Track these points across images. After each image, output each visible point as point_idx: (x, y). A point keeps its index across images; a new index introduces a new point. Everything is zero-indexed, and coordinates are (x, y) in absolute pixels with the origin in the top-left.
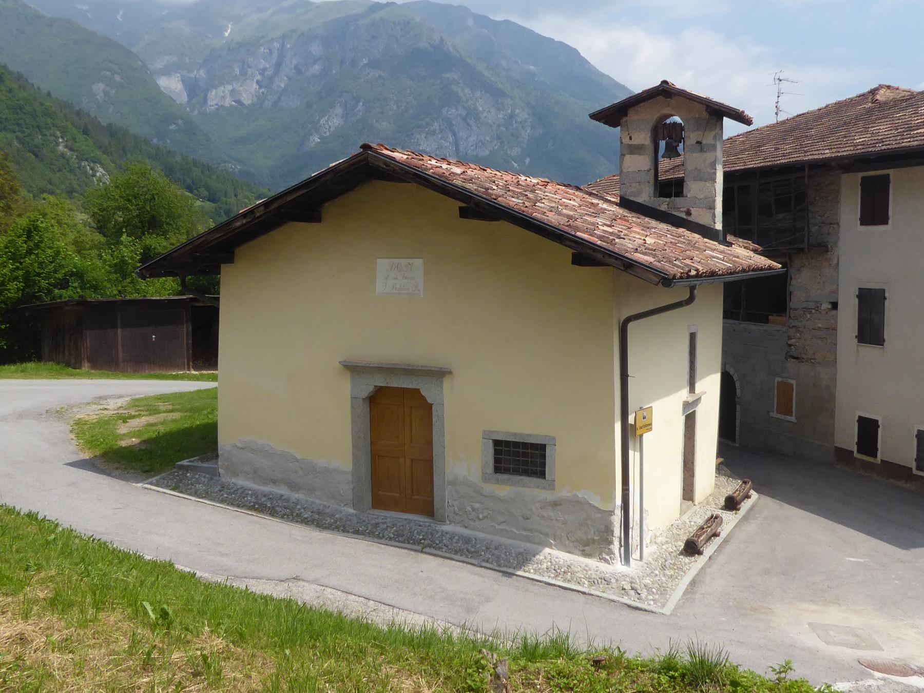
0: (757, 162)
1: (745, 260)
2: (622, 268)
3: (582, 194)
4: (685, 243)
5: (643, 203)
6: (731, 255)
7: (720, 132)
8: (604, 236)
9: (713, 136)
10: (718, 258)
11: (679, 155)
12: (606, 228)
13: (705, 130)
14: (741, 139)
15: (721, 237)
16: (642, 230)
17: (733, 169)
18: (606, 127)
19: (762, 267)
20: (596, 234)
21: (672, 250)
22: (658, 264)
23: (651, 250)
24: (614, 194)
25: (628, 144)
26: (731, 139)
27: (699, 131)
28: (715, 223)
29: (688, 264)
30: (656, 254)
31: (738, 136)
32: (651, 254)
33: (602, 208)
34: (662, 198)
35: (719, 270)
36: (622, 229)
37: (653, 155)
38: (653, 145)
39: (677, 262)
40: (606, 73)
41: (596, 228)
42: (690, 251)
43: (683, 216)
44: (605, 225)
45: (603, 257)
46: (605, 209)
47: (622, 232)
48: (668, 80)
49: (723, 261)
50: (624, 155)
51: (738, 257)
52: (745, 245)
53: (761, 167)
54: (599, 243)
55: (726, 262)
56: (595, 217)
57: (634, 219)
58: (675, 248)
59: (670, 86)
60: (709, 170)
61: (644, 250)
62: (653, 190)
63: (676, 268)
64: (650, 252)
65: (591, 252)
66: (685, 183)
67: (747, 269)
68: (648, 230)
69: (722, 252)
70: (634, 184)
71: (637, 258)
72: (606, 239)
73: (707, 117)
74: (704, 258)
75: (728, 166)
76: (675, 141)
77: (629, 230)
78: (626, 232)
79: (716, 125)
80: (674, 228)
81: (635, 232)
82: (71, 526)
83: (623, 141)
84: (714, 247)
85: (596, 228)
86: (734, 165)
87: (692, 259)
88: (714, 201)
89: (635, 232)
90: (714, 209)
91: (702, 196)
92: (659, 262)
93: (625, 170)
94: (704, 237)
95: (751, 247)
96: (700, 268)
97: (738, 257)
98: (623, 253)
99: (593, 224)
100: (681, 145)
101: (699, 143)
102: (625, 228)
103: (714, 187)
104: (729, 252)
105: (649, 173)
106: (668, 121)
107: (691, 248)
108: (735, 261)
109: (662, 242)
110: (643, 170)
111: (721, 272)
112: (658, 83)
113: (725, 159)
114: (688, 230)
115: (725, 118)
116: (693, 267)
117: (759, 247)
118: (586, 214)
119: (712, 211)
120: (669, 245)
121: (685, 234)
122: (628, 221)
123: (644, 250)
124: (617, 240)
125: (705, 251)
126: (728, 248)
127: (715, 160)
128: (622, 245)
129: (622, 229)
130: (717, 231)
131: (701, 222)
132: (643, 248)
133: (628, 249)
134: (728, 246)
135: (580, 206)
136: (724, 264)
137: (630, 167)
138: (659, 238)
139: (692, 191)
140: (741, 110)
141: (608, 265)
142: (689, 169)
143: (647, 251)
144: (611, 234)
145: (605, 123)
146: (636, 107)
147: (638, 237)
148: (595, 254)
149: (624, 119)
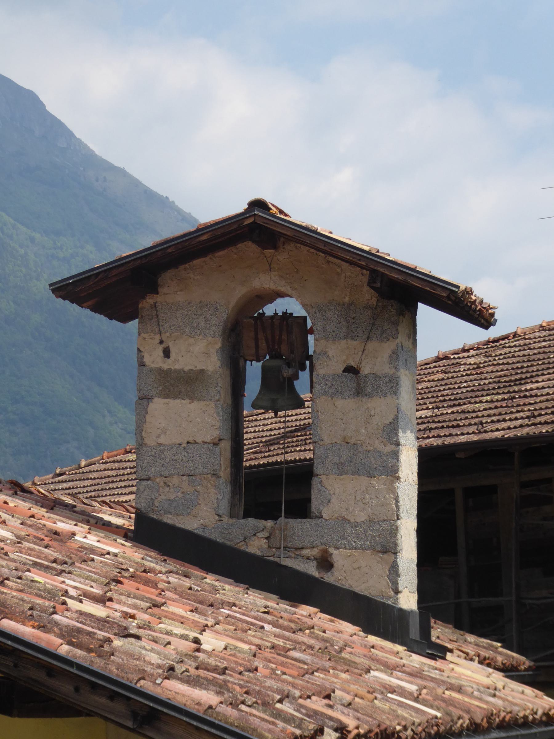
0: (512, 424)
1: (480, 699)
2: (130, 724)
3: (28, 505)
4: (312, 647)
5: (200, 532)
6: (439, 682)
7: (408, 344)
8: (80, 631)
9: (389, 352)
10: (402, 692)
11: (300, 404)
12: (89, 607)
13: (368, 338)
14: (472, 360)
15: (414, 633)
16: (194, 610)
17: (449, 441)
18: (100, 320)
19: (525, 717)
20: (57, 624)
21: (273, 671)
22: (230, 711)
23: (215, 670)
24: (118, 503)
25: (160, 370)
26: (446, 358)
27: (353, 338)
28: (397, 592)
29: (316, 712)
30: (225, 681)
31: (464, 350)
32: (213, 682)
33: (82, 547)
34: (252, 521)
35: (405, 728)
36: (135, 607)
37: (229, 401)
38: (227, 372)
39: (286, 707)
40: (117, 163)
41: (59, 607)
42: (325, 670)
43: (312, 570)
44: (87, 595)
45: (77, 689)
46: (92, 550)
47: (133, 617)
48: (269, 199)
49: (416, 700)
50: (149, 399)
51: (459, 689)
52: (484, 653)
53: (522, 438)
54: (64, 649)
55: (425, 703)
56: (60, 573)
57: (173, 579)
58: (283, 664)
59: (273, 215)
60: (381, 447)
61: (192, 671)
62: (228, 496)
63: (281, 724)
64: (211, 675)
65: (41, 676)
66: (315, 480)
67: (485, 724)
68: (210, 611)
69: (416, 674)
70: (175, 480)
71: (170, 695)
72: (85, 639)
73: (374, 301)
74: (363, 691)
75: (435, 433)
76: (289, 365)
77: (156, 610)
78: (146, 617)
79: (396, 324)
80: (284, 606)
81: (173, 617)
82: (286, 310)
83: (147, 360)
84: (393, 659)
85: (59, 607)
86: (454, 431)
87: (328, 697)
88: (394, 531)
89: (173, 617)
90: (395, 553)
91: (361, 517)
92: (234, 705)
93: (150, 441)
94: (369, 629)
95: (500, 659)
96: (351, 723)
97: (459, 689)
98: (131, 679)
99: (51, 594)
100: (304, 376)
101: (350, 370)
102: (145, 605)
103: (393, 491)
104: (435, 674)
105: (217, 450)
106: (269, 310)
107: (328, 664)
108: (450, 702)
109: (246, 647)
110: (200, 440)
111: (409, 732)
112: (240, 207)
113: (429, 413)
114: (322, 611)
115: (422, 307)
116: (331, 718)
117: (522, 658)
118: (35, 564)
119: (390, 557)
120: (268, 654)
121: (315, 620)
122: (155, 585)
123: (192, 671)
124: (118, 643)
125: (368, 671)
126: (432, 662)
127: (396, 418)
128: (131, 655)
129: (135, 607)
130: (403, 614)
131: (360, 588)
132: (190, 665)
133: (148, 669)
134: (432, 657)
135: (20, 540)
136: (417, 710)
137: (164, 431)
138: (240, 634)
139: (333, 500)
140: (462, 288)
141: (89, 714)
142: (327, 441)
143: (201, 672)
144: (103, 623)
145: (96, 309)
146: (182, 267)
147: (178, 630)
148: (52, 682)
149: (150, 300)
